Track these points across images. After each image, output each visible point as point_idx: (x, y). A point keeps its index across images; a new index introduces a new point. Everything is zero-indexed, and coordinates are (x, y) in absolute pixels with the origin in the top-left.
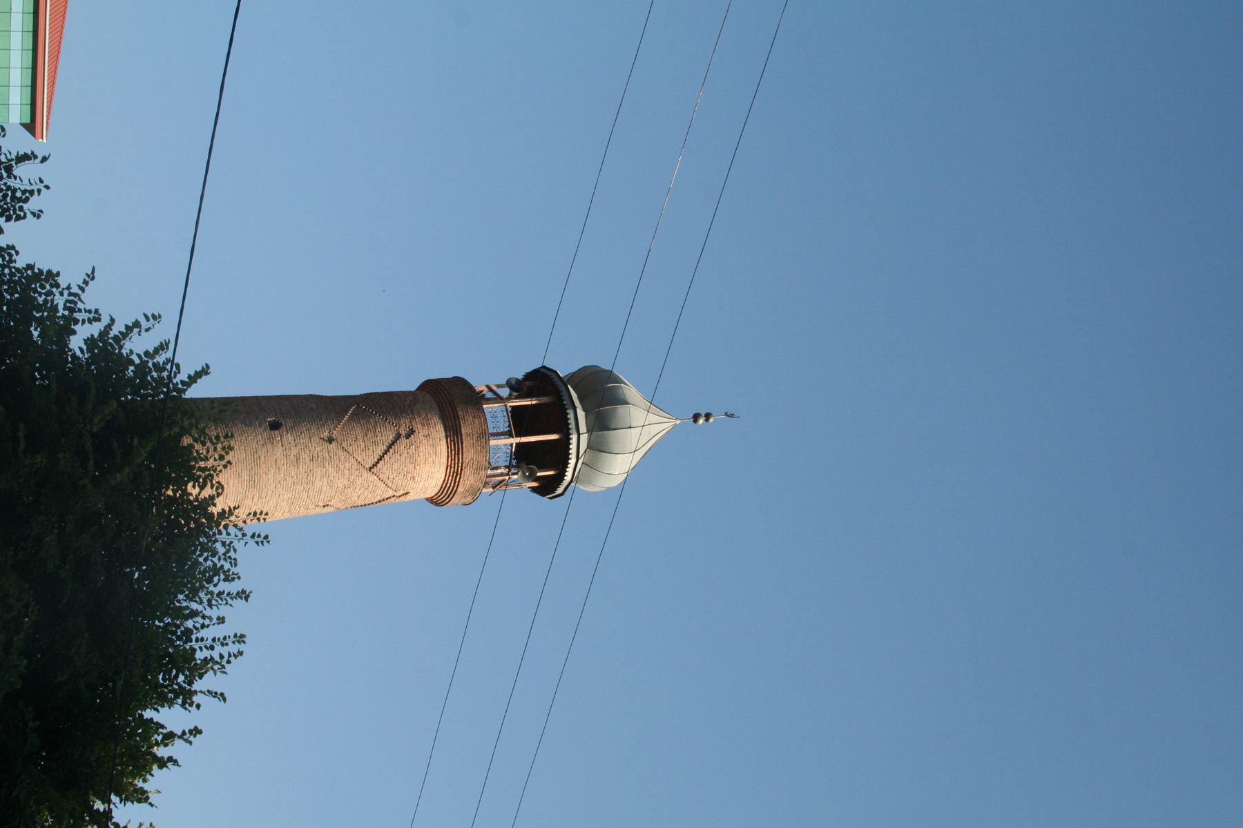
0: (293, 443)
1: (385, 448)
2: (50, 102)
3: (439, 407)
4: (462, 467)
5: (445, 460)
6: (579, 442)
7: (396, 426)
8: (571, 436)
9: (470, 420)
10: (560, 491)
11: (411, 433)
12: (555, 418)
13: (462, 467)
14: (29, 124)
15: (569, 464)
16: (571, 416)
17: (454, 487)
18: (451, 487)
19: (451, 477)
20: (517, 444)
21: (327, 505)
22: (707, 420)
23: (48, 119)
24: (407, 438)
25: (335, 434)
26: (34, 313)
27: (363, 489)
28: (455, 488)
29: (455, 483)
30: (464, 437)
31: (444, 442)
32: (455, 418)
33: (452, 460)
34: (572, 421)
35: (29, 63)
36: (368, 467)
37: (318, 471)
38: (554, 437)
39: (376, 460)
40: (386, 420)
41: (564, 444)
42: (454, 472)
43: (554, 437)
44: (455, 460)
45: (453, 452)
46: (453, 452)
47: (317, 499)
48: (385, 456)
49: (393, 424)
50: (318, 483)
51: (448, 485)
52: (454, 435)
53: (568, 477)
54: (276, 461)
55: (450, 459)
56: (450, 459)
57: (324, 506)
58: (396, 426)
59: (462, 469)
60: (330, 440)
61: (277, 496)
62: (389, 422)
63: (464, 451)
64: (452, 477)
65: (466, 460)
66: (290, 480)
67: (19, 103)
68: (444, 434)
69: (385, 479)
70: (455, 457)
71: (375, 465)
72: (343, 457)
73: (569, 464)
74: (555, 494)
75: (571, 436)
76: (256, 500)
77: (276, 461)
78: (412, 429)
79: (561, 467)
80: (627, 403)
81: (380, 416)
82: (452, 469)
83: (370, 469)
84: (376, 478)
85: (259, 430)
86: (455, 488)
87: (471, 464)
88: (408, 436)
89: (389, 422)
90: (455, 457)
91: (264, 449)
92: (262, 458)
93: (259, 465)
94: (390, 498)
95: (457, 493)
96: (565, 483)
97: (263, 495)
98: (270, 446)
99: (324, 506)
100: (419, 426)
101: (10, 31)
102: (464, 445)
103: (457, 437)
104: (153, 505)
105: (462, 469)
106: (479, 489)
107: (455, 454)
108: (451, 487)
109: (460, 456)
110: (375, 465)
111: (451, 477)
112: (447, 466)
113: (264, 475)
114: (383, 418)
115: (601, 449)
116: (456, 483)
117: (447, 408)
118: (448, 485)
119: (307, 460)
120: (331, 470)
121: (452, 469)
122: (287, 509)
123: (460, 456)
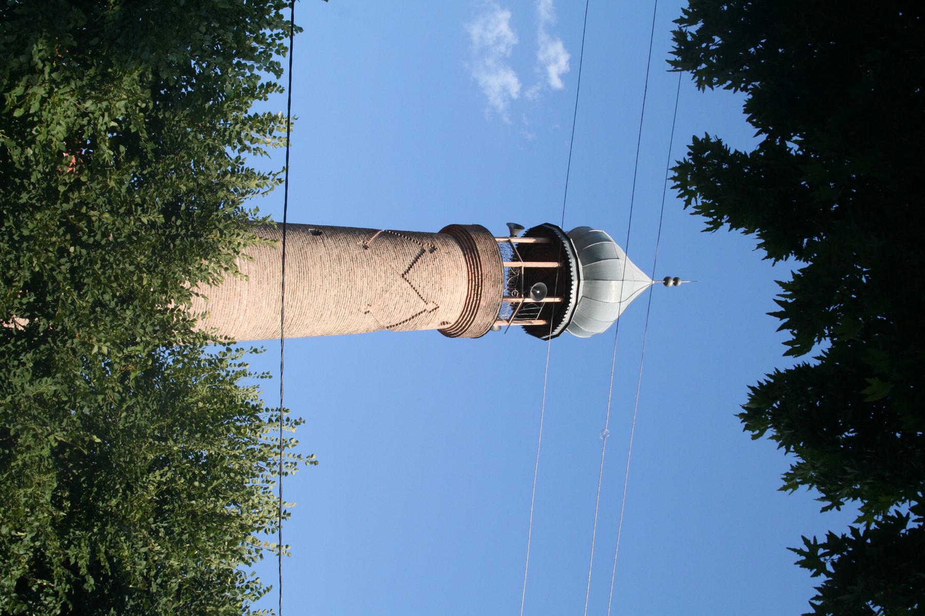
0: (333, 245)
1: (413, 259)
3: (454, 236)
4: (482, 278)
5: (465, 274)
6: (577, 289)
7: (420, 244)
8: (570, 261)
9: (483, 240)
11: (433, 250)
13: (482, 278)
15: (564, 318)
17: (476, 300)
18: (474, 302)
19: (473, 291)
20: (525, 268)
21: (368, 312)
22: (675, 284)
24: (431, 253)
25: (369, 243)
27: (399, 297)
28: (478, 301)
29: (477, 297)
30: (480, 252)
31: (463, 259)
32: (469, 240)
33: (472, 273)
36: (401, 274)
37: (359, 272)
39: (407, 268)
40: (411, 239)
42: (475, 285)
44: (474, 273)
45: (472, 266)
46: (472, 266)
47: (359, 299)
48: (415, 264)
49: (417, 242)
50: (359, 284)
51: (471, 300)
53: (573, 301)
54: (321, 258)
55: (470, 273)
56: (470, 273)
57: (365, 313)
58: (420, 244)
59: (482, 281)
60: (366, 247)
61: (324, 291)
62: (414, 241)
63: (482, 264)
64: (474, 291)
65: (485, 272)
66: (334, 276)
68: (462, 253)
70: (474, 270)
71: (407, 271)
72: (378, 261)
73: (564, 318)
75: (570, 261)
76: (306, 292)
77: (321, 258)
78: (434, 247)
79: (564, 295)
81: (404, 237)
82: (474, 282)
85: (303, 234)
86: (478, 301)
88: (431, 252)
89: (414, 241)
90: (474, 270)
91: (310, 247)
92: (309, 253)
93: (306, 258)
94: (422, 312)
95: (480, 306)
96: (572, 305)
97: (313, 288)
98: (314, 246)
99: (365, 313)
100: (440, 246)
102: (481, 259)
103: (474, 253)
104: (221, 49)
105: (482, 281)
106: (499, 305)
107: (474, 268)
108: (474, 302)
109: (479, 269)
110: (407, 271)
111: (473, 291)
112: (469, 280)
113: (312, 268)
114: (407, 238)
115: (596, 278)
116: (478, 295)
117: (461, 235)
118: (471, 300)
119: (348, 259)
120: (370, 272)
121: (474, 282)
122: (334, 309)
123: (479, 269)
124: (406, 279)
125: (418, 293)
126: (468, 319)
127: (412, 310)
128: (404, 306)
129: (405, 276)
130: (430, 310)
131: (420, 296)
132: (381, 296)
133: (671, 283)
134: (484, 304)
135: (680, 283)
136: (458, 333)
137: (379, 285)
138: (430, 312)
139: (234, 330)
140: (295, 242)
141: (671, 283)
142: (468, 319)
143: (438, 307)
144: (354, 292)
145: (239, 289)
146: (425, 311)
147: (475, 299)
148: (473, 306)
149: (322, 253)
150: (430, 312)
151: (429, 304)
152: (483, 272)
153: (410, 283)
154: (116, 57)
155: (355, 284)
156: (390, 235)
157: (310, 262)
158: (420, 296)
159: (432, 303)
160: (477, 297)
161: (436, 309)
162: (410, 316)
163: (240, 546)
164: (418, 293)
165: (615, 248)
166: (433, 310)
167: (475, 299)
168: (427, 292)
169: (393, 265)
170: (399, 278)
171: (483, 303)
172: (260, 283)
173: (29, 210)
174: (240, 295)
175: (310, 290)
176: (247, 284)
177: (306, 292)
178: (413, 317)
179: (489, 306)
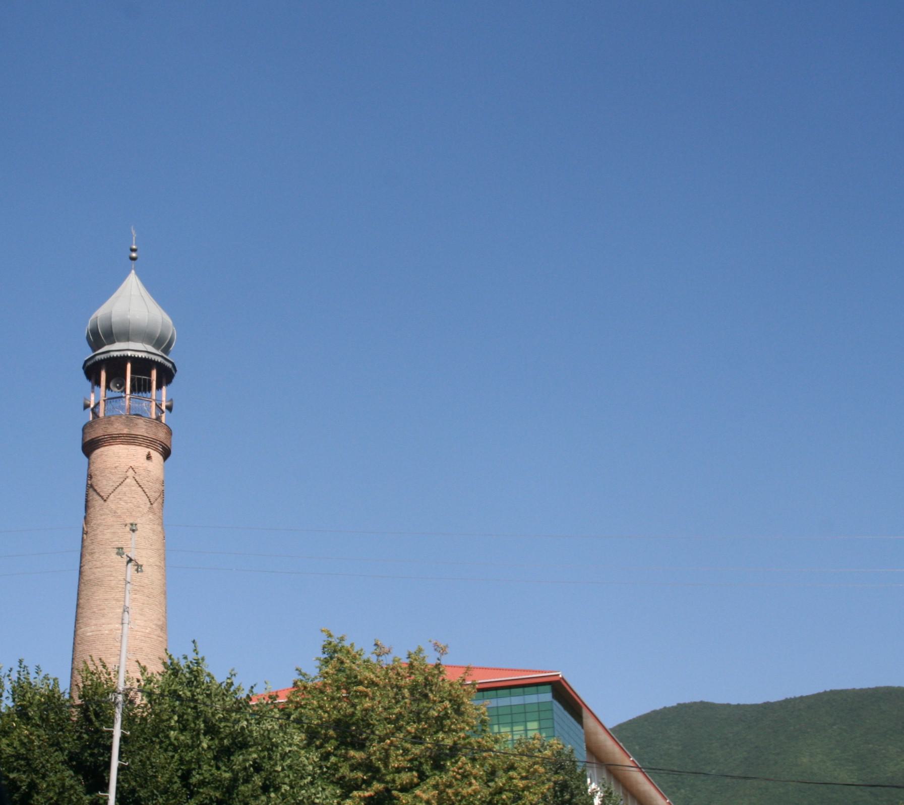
2: (536, 672)
5: (106, 448)
10: (170, 365)
12: (115, 366)
14: (552, 687)
16: (115, 354)
17: (124, 437)
23: (545, 672)
26: (104, 727)
28: (124, 435)
29: (121, 437)
34: (118, 354)
35: (534, 689)
38: (129, 366)
41: (135, 361)
43: (129, 366)
50: (108, 536)
52: (101, 442)
67: (512, 704)
69: (113, 488)
71: (102, 497)
74: (172, 369)
80: (112, 312)
83: (105, 501)
84: (112, 495)
87: (105, 430)
95: (128, 433)
101: (538, 703)
105: (108, 435)
110: (102, 497)
124: (107, 498)
125: (118, 486)
126: (142, 440)
127: (133, 488)
128: (130, 495)
129: (105, 498)
130: (134, 473)
131: (120, 484)
132: (120, 517)
133: (134, 255)
134: (127, 430)
135: (134, 247)
136: (159, 444)
137: (110, 519)
138: (135, 473)
139: (143, 630)
140: (80, 589)
141: (134, 255)
142: (142, 440)
143: (131, 467)
144: (114, 539)
145: (107, 632)
146: (134, 477)
147: (123, 438)
148: (129, 438)
149: (87, 567)
150: (135, 473)
151: (128, 476)
152: (102, 435)
153: (110, 494)
154: (98, 671)
155: (108, 539)
156: (87, 507)
157: (92, 577)
158: (120, 484)
159: (127, 473)
160: (121, 437)
161: (133, 469)
162: (139, 488)
163: (155, 679)
164: (118, 486)
165: (101, 313)
166: (134, 471)
167: (123, 438)
168: (116, 479)
169: (98, 509)
170: (106, 504)
171: (125, 431)
172: (103, 616)
173: (376, 690)
174: (111, 630)
175: (111, 576)
176: (104, 626)
177: (112, 578)
178: (140, 486)
179: (127, 425)
